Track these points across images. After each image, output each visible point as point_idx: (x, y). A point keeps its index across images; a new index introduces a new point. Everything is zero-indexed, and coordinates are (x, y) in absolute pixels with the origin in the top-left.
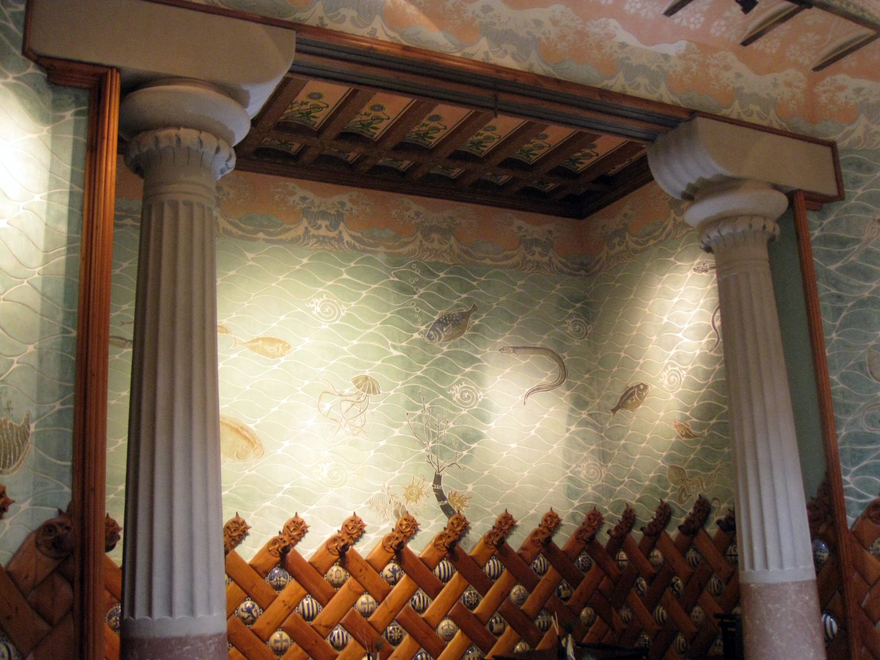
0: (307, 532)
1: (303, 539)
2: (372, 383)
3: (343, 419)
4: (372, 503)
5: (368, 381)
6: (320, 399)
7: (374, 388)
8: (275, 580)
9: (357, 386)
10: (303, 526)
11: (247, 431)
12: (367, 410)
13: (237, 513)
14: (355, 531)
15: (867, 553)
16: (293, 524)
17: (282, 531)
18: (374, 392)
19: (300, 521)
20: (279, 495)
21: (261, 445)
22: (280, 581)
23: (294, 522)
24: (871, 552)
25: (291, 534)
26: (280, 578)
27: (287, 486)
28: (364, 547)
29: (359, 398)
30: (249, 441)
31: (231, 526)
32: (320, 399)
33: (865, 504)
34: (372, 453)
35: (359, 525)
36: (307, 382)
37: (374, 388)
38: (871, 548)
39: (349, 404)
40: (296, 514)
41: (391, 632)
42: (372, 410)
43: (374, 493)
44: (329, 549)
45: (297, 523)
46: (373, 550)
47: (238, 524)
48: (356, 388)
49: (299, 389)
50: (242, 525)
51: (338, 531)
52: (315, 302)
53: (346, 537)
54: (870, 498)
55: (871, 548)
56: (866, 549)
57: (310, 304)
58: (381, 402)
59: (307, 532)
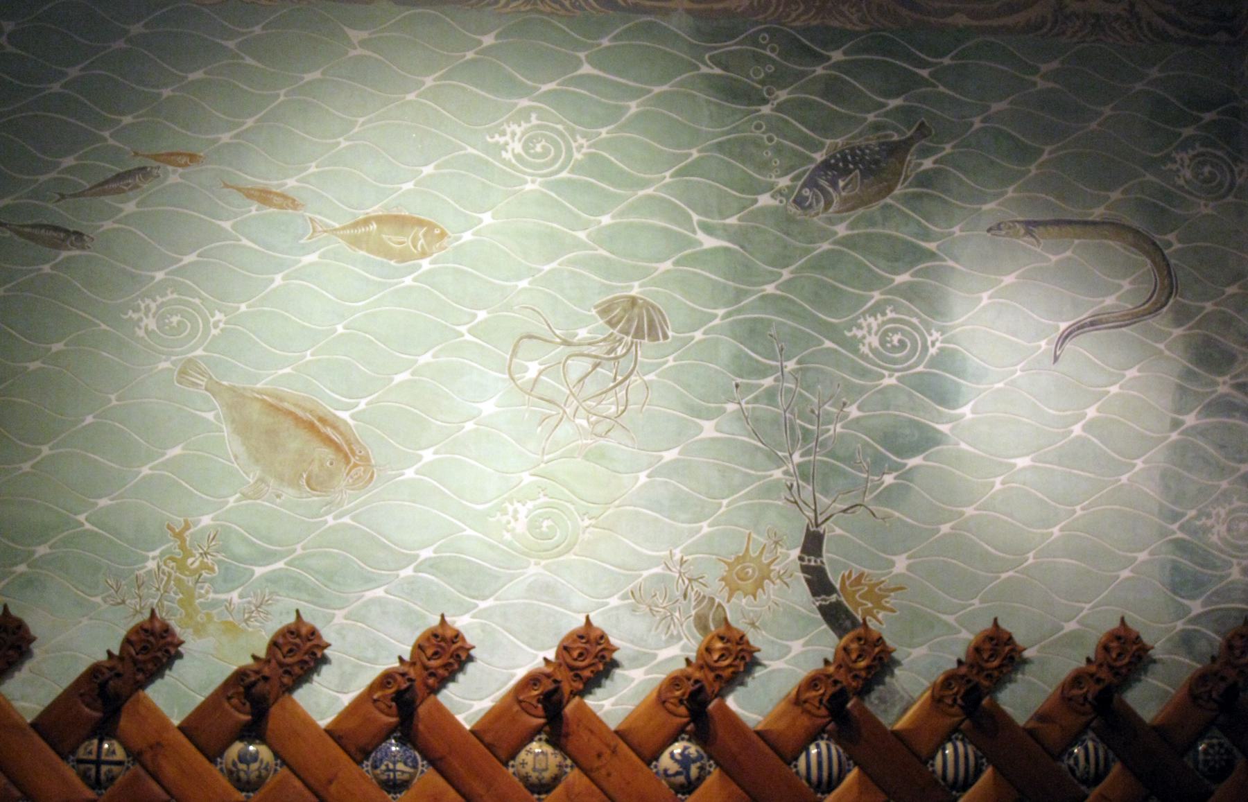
1: (461, 677)
2: (648, 311)
3: (571, 398)
4: (637, 594)
5: (636, 310)
6: (514, 353)
7: (652, 325)
10: (459, 644)
11: (334, 427)
12: (633, 378)
13: (297, 611)
18: (653, 335)
19: (449, 634)
20: (408, 572)
21: (366, 459)
23: (436, 636)
26: (394, 763)
27: (426, 553)
28: (612, 700)
29: (613, 350)
30: (338, 448)
31: (281, 641)
32: (514, 353)
34: (643, 478)
36: (482, 315)
37: (652, 325)
39: (586, 364)
40: (443, 616)
42: (646, 378)
43: (645, 574)
44: (520, 702)
45: (444, 639)
49: (463, 329)
50: (454, 643)
51: (545, 659)
52: (143, 306)
53: (563, 675)
57: (130, 312)
58: (671, 358)
59: (470, 659)
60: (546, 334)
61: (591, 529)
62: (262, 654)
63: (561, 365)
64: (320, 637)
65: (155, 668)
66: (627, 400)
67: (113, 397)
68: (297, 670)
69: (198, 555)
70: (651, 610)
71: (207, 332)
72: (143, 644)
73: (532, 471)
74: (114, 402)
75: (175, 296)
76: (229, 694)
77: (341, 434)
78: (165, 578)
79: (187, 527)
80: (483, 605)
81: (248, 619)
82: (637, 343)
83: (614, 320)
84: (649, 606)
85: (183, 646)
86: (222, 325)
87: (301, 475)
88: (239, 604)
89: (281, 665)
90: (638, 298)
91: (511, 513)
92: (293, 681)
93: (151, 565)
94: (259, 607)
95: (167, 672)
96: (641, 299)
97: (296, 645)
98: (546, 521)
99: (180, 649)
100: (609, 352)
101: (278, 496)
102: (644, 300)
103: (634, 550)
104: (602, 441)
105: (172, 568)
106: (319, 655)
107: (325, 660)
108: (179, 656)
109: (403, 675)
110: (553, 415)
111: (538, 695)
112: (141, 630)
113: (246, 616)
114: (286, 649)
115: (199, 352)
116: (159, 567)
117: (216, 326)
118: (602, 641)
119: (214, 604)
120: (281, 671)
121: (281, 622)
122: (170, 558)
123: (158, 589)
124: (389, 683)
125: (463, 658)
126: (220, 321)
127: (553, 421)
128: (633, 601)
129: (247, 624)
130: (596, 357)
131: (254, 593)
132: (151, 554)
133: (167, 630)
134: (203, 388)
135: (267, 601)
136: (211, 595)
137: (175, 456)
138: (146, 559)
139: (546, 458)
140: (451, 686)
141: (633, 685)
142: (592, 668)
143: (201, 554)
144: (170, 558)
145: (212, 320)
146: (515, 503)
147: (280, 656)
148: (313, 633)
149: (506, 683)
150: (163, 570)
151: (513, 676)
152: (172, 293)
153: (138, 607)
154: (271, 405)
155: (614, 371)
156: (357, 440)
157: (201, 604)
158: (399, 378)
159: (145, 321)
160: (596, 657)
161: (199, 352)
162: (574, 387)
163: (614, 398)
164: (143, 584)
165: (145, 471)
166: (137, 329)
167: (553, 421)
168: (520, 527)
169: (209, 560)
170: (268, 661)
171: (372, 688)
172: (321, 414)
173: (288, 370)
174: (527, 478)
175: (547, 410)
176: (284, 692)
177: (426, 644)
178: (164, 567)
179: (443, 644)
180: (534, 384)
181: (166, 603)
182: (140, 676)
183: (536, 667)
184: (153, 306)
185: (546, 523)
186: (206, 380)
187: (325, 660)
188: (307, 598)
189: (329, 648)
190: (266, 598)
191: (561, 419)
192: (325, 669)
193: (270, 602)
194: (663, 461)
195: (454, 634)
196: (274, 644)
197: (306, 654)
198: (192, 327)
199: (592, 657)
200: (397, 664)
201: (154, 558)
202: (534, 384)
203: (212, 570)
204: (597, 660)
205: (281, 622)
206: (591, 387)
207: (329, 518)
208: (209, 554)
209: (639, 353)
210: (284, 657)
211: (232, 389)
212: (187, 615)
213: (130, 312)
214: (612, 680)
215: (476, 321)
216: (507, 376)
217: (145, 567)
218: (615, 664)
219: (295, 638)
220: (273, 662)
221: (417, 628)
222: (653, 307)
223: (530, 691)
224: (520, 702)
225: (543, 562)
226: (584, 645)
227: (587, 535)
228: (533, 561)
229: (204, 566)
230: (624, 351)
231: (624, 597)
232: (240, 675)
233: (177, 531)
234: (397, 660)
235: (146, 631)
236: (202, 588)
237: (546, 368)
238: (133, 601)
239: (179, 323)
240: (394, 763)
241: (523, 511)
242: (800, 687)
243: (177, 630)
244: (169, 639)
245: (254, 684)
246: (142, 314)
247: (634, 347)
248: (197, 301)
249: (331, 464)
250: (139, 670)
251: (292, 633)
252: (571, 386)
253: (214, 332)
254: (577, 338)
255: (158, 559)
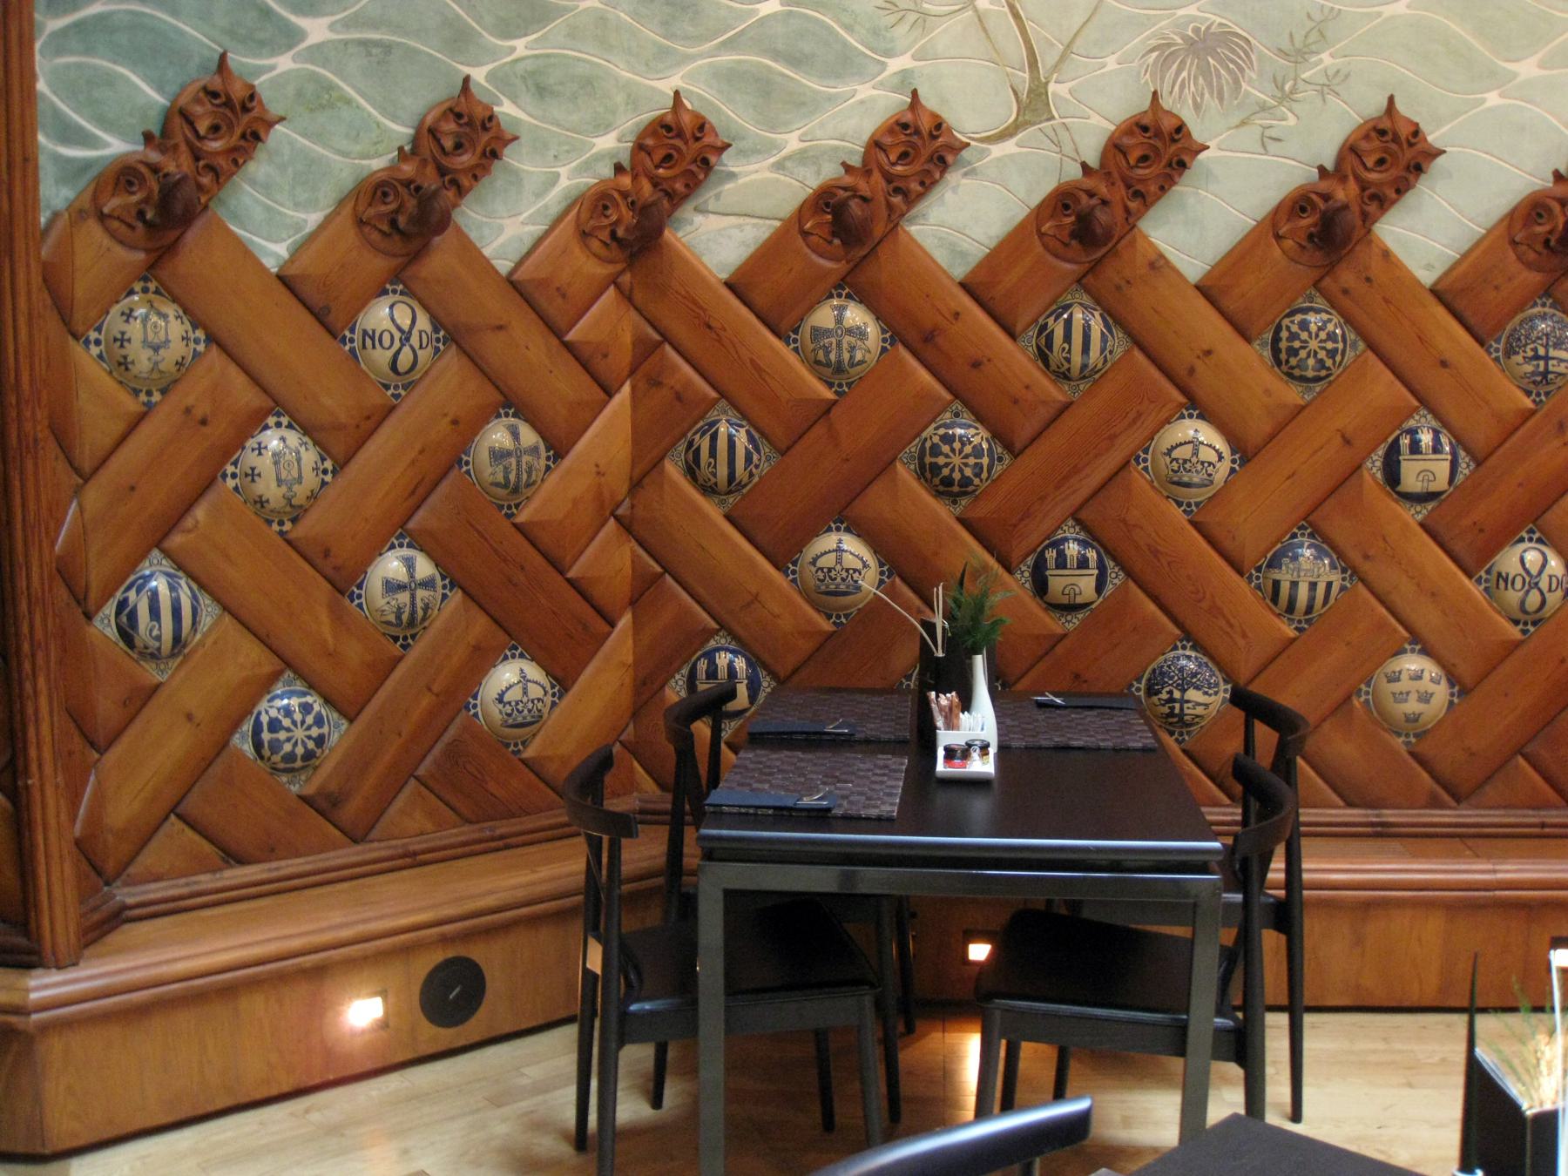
8: (1164, 696)
15: (77, 348)
22: (1547, 358)
24: (95, 350)
25: (445, 161)
31: (650, 142)
33: (87, 165)
35: (485, 137)
38: (93, 335)
41: (274, 725)
47: (1396, 139)
54: (106, 145)
55: (93, 335)
56: (76, 337)
72: (902, 149)
109: (1326, 197)
111: (1309, 226)
112: (900, 126)
114: (658, 156)
124: (1540, 215)
195: (1412, 129)
240: (1546, 347)
242: (802, 206)
244: (707, 140)
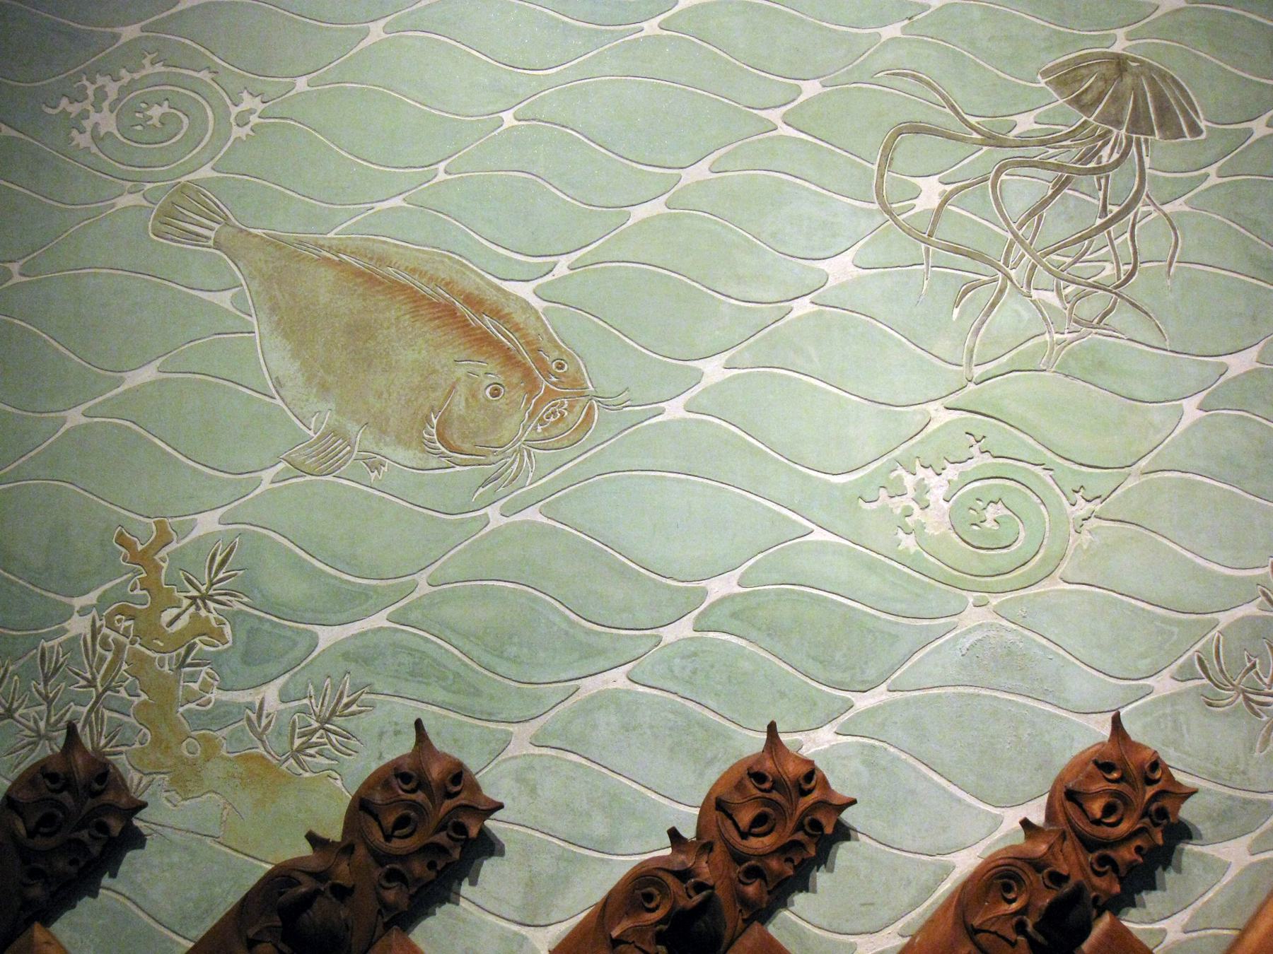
0: (844, 833)
1: (821, 878)
2: (1152, 82)
3: (1018, 249)
4: (1213, 666)
5: (1128, 80)
6: (887, 160)
7: (1164, 109)
9: (1077, 102)
10: (814, 796)
11: (497, 314)
12: (1141, 208)
13: (418, 724)
14: (1124, 827)
16: (750, 785)
17: (689, 833)
18: (1169, 126)
19: (792, 770)
20: (683, 630)
21: (576, 385)
23: (759, 777)
27: (719, 588)
28: (1183, 917)
29: (1093, 154)
30: (509, 359)
31: (378, 798)
32: (887, 160)
34: (1191, 409)
35: (1150, 791)
36: (811, 89)
37: (1164, 109)
39: (1041, 182)
40: (772, 729)
42: (1167, 208)
43: (1225, 619)
44: (973, 932)
45: (778, 784)
46: (1244, 932)
48: (1074, 110)
49: (775, 115)
50: (804, 793)
51: (1026, 824)
52: (91, 90)
53: (1072, 862)
57: (64, 102)
58: (1212, 170)
59: (844, 833)
60: (954, 126)
61: (1094, 522)
62: (334, 832)
63: (989, 183)
64: (475, 788)
65: (73, 870)
66: (1135, 253)
67: (15, 268)
68: (418, 868)
69: (186, 602)
70: (1247, 700)
71: (222, 133)
72: (401, 812)
73: (950, 401)
74: (17, 279)
75: (159, 68)
76: (251, 933)
77: (516, 328)
78: (110, 656)
79: (163, 539)
80: (863, 702)
81: (300, 750)
82: (1138, 140)
83: (1088, 98)
84: (1244, 692)
85: (143, 814)
86: (254, 119)
87: (429, 421)
88: (280, 712)
89: (380, 858)
90: (1127, 58)
91: (911, 493)
92: (411, 897)
93: (78, 626)
94: (328, 721)
95: (106, 880)
96: (1135, 60)
97: (414, 805)
98: (991, 508)
99: (488, 823)
100: (1085, 158)
101: (375, 467)
102: (1142, 63)
103: (1196, 567)
104: (1093, 337)
105: (126, 635)
106: (473, 832)
107: (488, 846)
108: (135, 839)
109: (683, 875)
110: (985, 283)
113: (297, 742)
114: (390, 819)
115: (206, 172)
116: (95, 632)
117: (242, 121)
118: (1158, 775)
119: (222, 715)
120: (377, 873)
121: (380, 757)
122: (120, 611)
123: (91, 683)
124: (649, 897)
125: (829, 830)
126: (251, 112)
127: (984, 295)
128: (1206, 681)
129: (299, 763)
130: (1059, 167)
131: (317, 689)
132: (78, 602)
133: (104, 775)
134: (211, 243)
135: (348, 705)
136: (215, 695)
137: (144, 385)
138: (67, 613)
139: (978, 372)
140: (799, 899)
141: (1226, 879)
142: (1138, 842)
143: (193, 598)
144: (120, 611)
145: (235, 111)
146: (920, 470)
147: (378, 837)
148: (458, 775)
149: (931, 890)
150: (105, 638)
151: (948, 869)
152: (153, 63)
153: (42, 724)
154: (359, 274)
155: (1101, 194)
156: (552, 340)
157: (189, 715)
158: (639, 213)
159: (95, 117)
160: (1146, 814)
161: (206, 172)
162: (1021, 226)
163: (1109, 248)
164: (56, 670)
165: (75, 417)
166: (75, 133)
167: (984, 295)
168: (935, 520)
169: (211, 614)
170: (347, 849)
171: (606, 911)
172: (471, 288)
173: (397, 202)
174: (941, 416)
175: (969, 270)
176: (387, 926)
177: (737, 798)
178: (105, 631)
179: (775, 795)
180: (934, 224)
181: (107, 713)
182: (37, 891)
183: (1002, 846)
184: (112, 89)
185: (991, 512)
186: (217, 226)
187: (488, 846)
188: (440, 695)
189: (498, 814)
190: (345, 700)
191: (1002, 291)
192: (489, 868)
193: (354, 708)
194: (1229, 375)
195: (804, 770)
196: (362, 806)
197: (442, 827)
198: (191, 126)
199: (1136, 815)
200: (306, 849)
201: (84, 611)
202: (934, 224)
203: (221, 635)
204: (1147, 820)
205: (380, 757)
206: (1056, 226)
207: (493, 512)
208: (211, 598)
209: (1147, 160)
210: (388, 838)
211: (275, 243)
212: (157, 741)
213: (64, 102)
214: (831, 870)
215: (801, 99)
216: (876, 206)
217: (65, 631)
218: (1183, 832)
219: (413, 791)
220: (361, 851)
221: (710, 763)
222: (1164, 76)
223: (996, 903)
224: (973, 932)
225: (995, 601)
226: (1114, 787)
227: (1086, 537)
228: (971, 598)
229: (201, 629)
230: (1116, 156)
231: (1183, 676)
232: (281, 878)
233: (140, 548)
234: (667, 841)
235: (53, 777)
236: (193, 678)
237: (957, 191)
238: (32, 712)
239: (164, 119)
241: (938, 488)
243: (133, 778)
244: (109, 797)
245: (306, 901)
246: (87, 105)
247: (1134, 149)
248: (205, 75)
249: (495, 393)
250: (35, 874)
251: (405, 778)
252: (1014, 226)
253: (237, 132)
254: (1015, 132)
255: (94, 612)
